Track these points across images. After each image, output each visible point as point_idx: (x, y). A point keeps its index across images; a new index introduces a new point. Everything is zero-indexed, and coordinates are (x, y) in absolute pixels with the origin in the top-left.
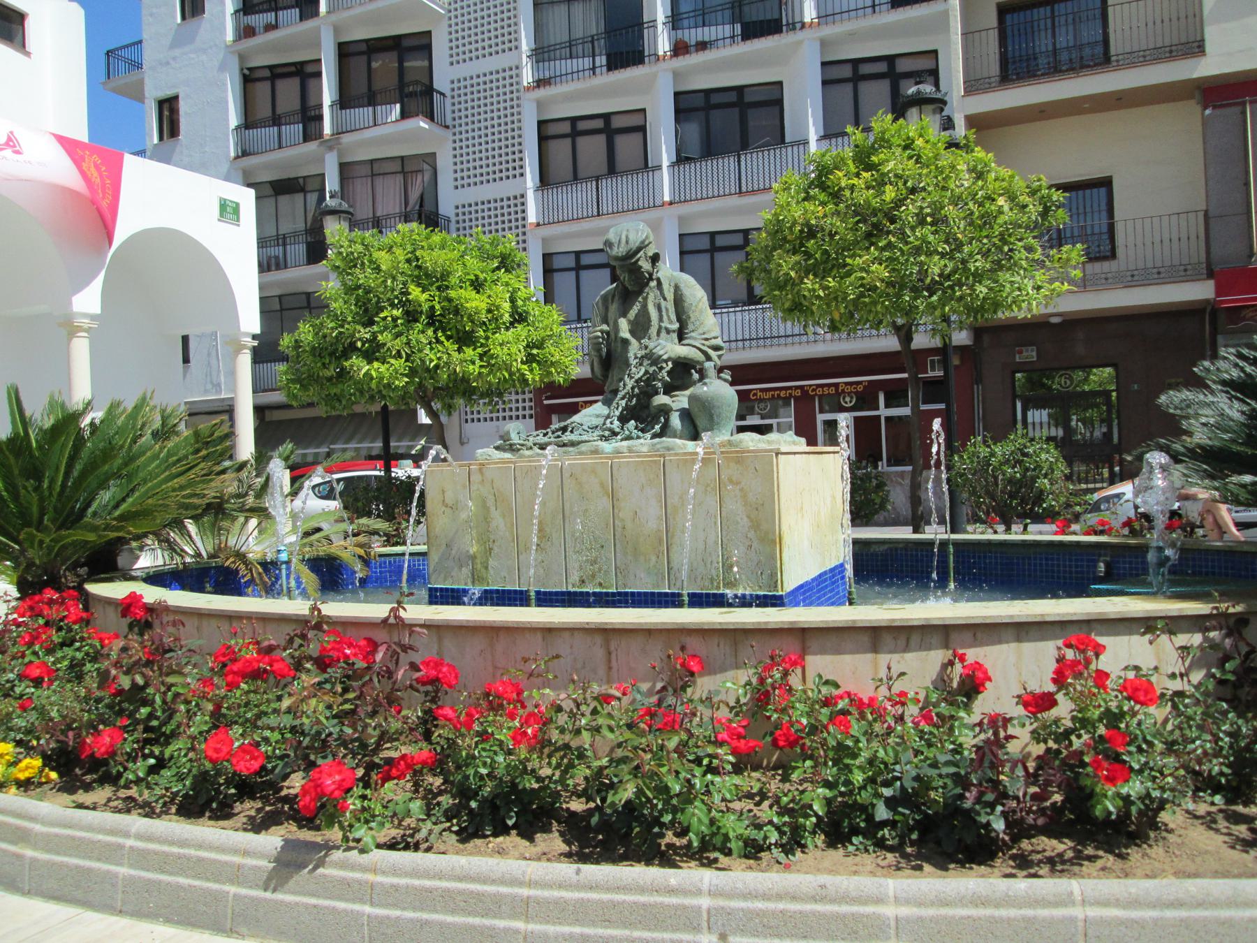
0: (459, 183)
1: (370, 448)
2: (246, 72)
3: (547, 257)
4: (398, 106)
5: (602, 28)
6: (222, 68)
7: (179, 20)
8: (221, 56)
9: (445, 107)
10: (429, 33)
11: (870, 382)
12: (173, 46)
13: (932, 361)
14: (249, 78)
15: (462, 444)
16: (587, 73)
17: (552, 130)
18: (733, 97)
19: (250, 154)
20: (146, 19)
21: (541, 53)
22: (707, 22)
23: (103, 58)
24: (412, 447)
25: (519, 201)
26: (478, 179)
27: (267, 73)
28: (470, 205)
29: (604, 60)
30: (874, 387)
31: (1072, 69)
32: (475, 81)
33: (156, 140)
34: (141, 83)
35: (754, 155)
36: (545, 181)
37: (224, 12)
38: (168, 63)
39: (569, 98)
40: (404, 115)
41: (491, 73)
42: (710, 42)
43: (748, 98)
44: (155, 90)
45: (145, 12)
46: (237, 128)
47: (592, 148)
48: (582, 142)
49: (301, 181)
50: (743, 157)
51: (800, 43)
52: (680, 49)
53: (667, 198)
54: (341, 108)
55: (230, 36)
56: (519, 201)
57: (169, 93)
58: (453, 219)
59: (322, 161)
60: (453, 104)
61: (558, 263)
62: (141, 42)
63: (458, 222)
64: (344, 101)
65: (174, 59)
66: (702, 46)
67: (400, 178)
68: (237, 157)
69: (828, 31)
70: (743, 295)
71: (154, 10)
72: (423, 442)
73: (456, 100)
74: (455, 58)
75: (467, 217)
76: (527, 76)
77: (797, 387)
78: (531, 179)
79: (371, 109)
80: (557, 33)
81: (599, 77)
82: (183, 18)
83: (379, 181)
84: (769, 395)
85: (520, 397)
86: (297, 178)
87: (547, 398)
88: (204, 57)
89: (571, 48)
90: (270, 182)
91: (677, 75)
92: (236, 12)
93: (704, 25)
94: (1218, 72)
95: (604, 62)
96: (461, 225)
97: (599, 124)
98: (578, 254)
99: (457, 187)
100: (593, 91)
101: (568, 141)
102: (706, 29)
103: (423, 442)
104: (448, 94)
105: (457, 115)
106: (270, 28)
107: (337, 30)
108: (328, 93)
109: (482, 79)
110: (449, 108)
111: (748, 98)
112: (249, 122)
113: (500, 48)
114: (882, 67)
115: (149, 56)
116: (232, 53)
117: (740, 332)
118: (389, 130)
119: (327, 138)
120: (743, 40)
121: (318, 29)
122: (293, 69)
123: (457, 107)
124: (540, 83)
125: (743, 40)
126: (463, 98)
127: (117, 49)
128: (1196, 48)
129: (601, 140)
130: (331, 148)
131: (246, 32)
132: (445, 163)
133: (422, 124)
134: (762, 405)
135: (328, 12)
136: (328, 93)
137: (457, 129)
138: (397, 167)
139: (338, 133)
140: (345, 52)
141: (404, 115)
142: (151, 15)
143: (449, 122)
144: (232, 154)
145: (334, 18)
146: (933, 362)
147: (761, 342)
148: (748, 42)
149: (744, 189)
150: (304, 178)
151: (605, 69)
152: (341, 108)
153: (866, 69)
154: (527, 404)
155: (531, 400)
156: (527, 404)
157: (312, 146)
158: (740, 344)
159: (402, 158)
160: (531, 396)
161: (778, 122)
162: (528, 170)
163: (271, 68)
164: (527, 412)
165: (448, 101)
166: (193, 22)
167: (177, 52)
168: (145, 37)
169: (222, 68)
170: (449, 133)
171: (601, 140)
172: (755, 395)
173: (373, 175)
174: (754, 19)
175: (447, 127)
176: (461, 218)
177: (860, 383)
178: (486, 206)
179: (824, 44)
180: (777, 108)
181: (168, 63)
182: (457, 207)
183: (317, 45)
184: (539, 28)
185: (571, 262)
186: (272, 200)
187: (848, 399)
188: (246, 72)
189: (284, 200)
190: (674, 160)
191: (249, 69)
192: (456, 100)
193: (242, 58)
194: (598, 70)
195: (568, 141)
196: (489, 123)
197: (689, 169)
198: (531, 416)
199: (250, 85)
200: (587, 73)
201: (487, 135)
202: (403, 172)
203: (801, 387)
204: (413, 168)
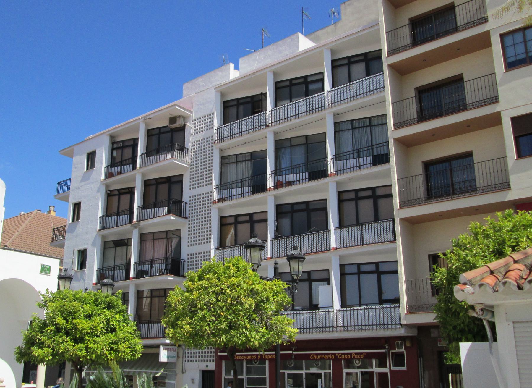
0: (190, 243)
1: (129, 372)
2: (109, 192)
3: (342, 266)
4: (167, 208)
5: (250, 175)
6: (98, 191)
7: (85, 170)
8: (98, 186)
9: (186, 209)
10: (182, 175)
11: (366, 353)
12: (82, 181)
13: (398, 344)
14: (110, 195)
15: (183, 372)
16: (355, 169)
17: (345, 196)
18: (304, 207)
19: (106, 229)
20: (74, 169)
21: (222, 187)
22: (293, 172)
23: (56, 185)
24: (157, 373)
25: (208, 254)
26: (198, 242)
27: (117, 193)
28: (194, 254)
29: (250, 189)
30: (369, 356)
31: (461, 193)
32: (199, 197)
33: (71, 221)
34: (68, 196)
35: (385, 223)
36: (222, 245)
37: (102, 167)
38: (79, 188)
39: (232, 206)
40: (169, 212)
41: (206, 194)
42: (294, 182)
43: (311, 207)
44: (73, 200)
45: (73, 166)
46: (102, 217)
47: (366, 206)
48: (240, 226)
49: (126, 241)
50: (302, 237)
51: (327, 183)
52: (278, 185)
53: (269, 256)
54: (143, 209)
55: (103, 177)
56: (208, 254)
57: (77, 201)
58: (186, 261)
59: (131, 232)
60: (190, 207)
61: (347, 270)
62: (70, 179)
63: (188, 262)
64: (145, 206)
65: (81, 186)
66: (290, 183)
67: (165, 241)
68: (100, 230)
69: (339, 178)
70: (307, 304)
71: (77, 166)
72: (162, 371)
73: (191, 205)
74: (192, 186)
75: (192, 260)
76: (215, 197)
77: (348, 354)
78: (213, 244)
79: (379, 153)
80: (231, 177)
81: (362, 170)
82: (87, 169)
83: (157, 242)
84: (319, 357)
85: (209, 350)
86: (123, 240)
87: (221, 352)
88: (92, 186)
89: (238, 183)
90: (113, 241)
91: (276, 197)
92: (107, 167)
93: (291, 174)
94: (517, 198)
95: (307, 177)
96: (190, 264)
97: (247, 218)
98: (359, 265)
99: (189, 246)
100: (245, 204)
101: (353, 203)
102: (292, 175)
103: (162, 371)
104: (188, 203)
105: (191, 212)
106: (120, 173)
107: (143, 175)
108: (137, 203)
109: (196, 197)
110: (188, 209)
111: (311, 207)
112: (108, 213)
113: (202, 184)
114: (369, 193)
115: (73, 184)
116: (103, 184)
117: (367, 321)
118: (163, 219)
119: (134, 223)
120: (373, 166)
121: (135, 174)
122: (127, 190)
123: (191, 208)
124: (220, 200)
125: (373, 166)
126: (194, 204)
127: (64, 181)
128: (506, 186)
129: (248, 225)
130: (136, 228)
131: (109, 175)
132: (185, 235)
133: (172, 218)
134: (317, 363)
135: (140, 167)
136: (137, 203)
137: (190, 219)
138: (164, 235)
139: (140, 220)
140: (147, 184)
141: (169, 212)
142: (76, 168)
143: (187, 215)
144: (98, 228)
145: (143, 170)
146: (398, 344)
147: (324, 329)
148: (310, 182)
149: (365, 243)
150: (128, 239)
151: (307, 180)
152: (143, 209)
153: (362, 194)
154: (212, 354)
155: (213, 353)
156: (212, 354)
157: (129, 226)
158: (367, 327)
159: (167, 231)
160: (214, 350)
161: (325, 218)
162: (212, 240)
163: (118, 190)
164: (212, 359)
165: (188, 206)
166: (90, 171)
167: (83, 183)
168: (72, 177)
169: (98, 191)
170: (187, 220)
171: (248, 225)
172: (313, 357)
173: (154, 239)
174: (382, 153)
175: (186, 218)
176: (190, 260)
177: (362, 353)
178: (200, 255)
179: (338, 184)
180: (325, 211)
181: (79, 188)
182: (188, 255)
183: (134, 180)
184: (222, 175)
185: (355, 270)
186: (114, 249)
187: (357, 362)
188: (109, 192)
189: (118, 249)
190: (273, 237)
191: (111, 191)
192: (191, 205)
193: (107, 186)
194: (362, 167)
195: (353, 203)
196: (203, 216)
197: (280, 242)
198: (213, 361)
199: (110, 198)
200: (355, 169)
201: (202, 222)
202: (167, 238)
203: (334, 354)
204: (172, 236)
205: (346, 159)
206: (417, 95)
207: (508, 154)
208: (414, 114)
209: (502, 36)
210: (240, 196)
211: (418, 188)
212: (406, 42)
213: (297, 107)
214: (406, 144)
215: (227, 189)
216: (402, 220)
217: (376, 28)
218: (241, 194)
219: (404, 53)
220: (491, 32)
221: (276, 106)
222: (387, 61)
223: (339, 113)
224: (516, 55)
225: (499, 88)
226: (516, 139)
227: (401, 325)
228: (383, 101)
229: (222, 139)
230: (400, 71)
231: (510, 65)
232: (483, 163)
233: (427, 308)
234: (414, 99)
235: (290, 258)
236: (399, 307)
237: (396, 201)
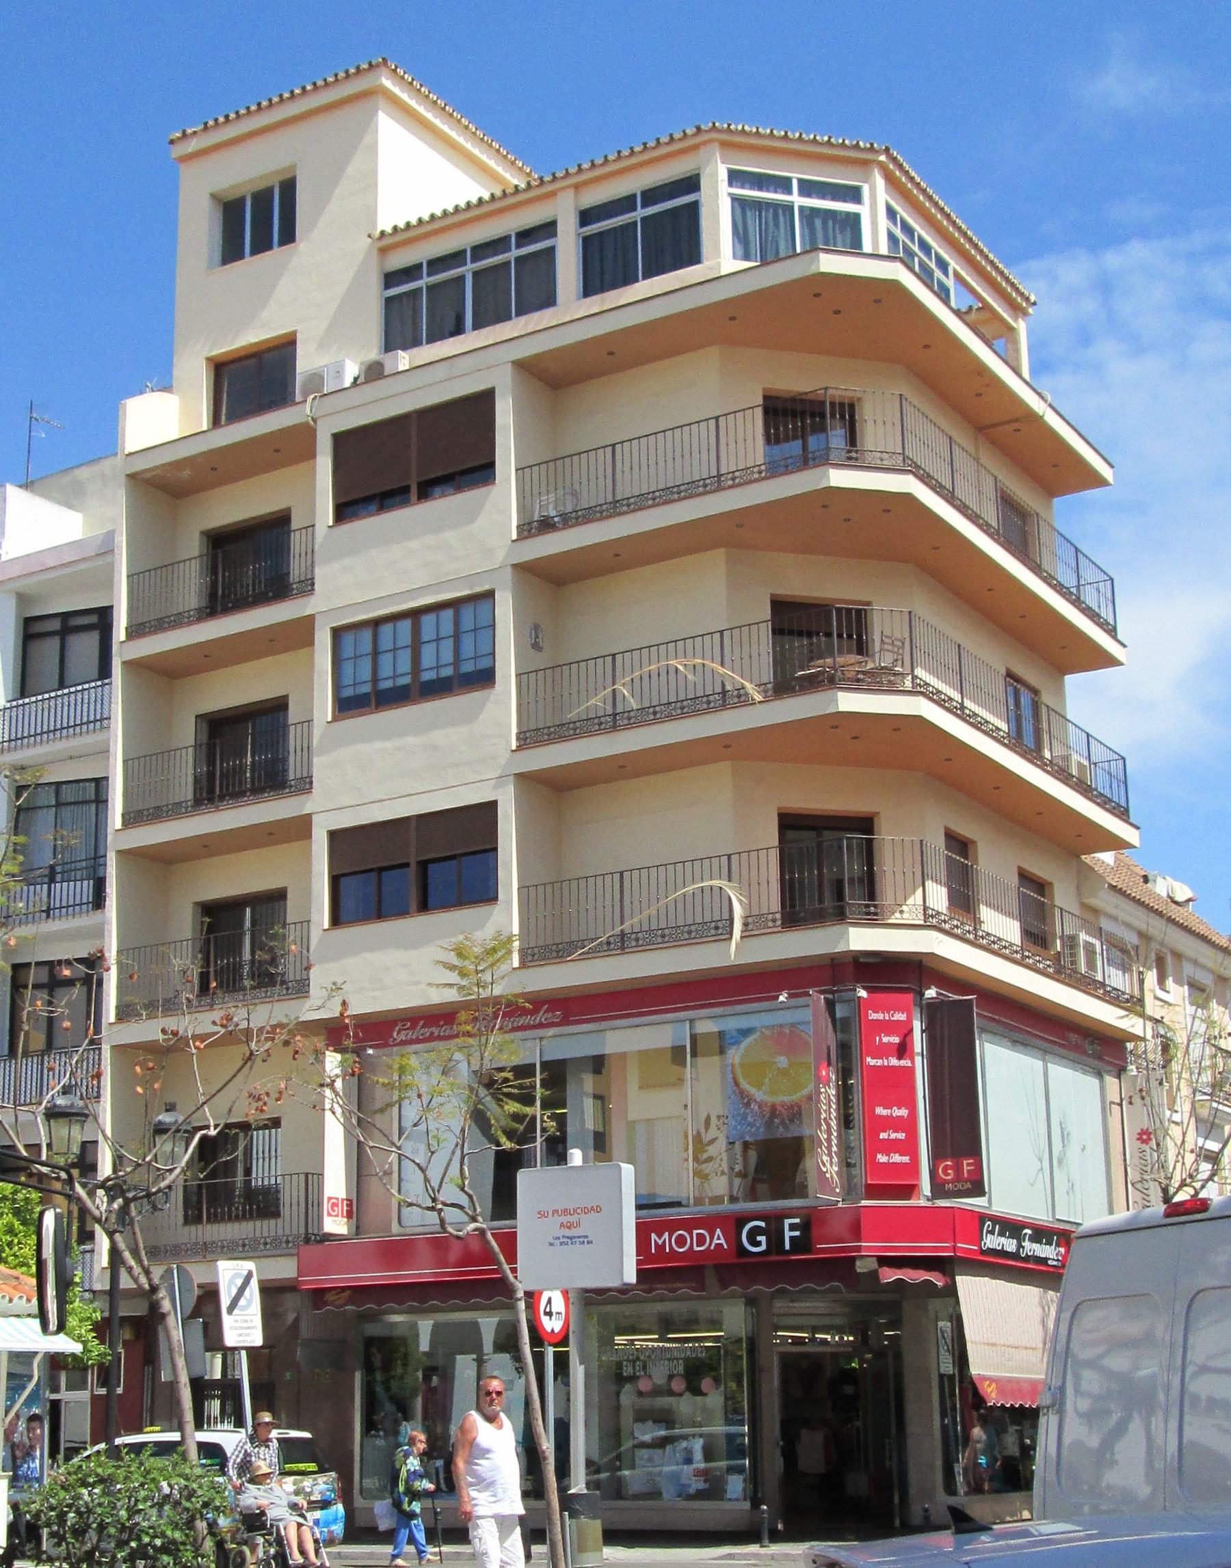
205: (75, 881)
206: (204, 738)
207: (314, 918)
208: (187, 792)
209: (337, 633)
210: (44, 915)
211: (600, 909)
212: (602, 495)
213: (73, 702)
214: (157, 864)
215: (69, 881)
216: (118, 1049)
217: (108, 558)
218: (48, 911)
219: (639, 514)
220: (317, 617)
221: (23, 695)
222: (123, 648)
223: (24, 763)
224: (438, 668)
225: (316, 761)
226: (335, 881)
227: (94, 1292)
228: (104, 752)
229: (16, 740)
230: (163, 675)
231: (346, 705)
232: (671, 868)
233: (223, 1247)
234: (191, 750)
235: (53, 1114)
236: (92, 1251)
237: (108, 1006)
